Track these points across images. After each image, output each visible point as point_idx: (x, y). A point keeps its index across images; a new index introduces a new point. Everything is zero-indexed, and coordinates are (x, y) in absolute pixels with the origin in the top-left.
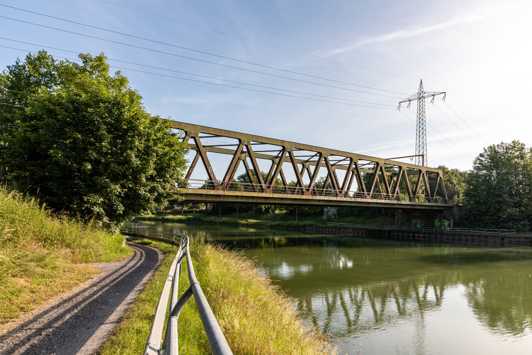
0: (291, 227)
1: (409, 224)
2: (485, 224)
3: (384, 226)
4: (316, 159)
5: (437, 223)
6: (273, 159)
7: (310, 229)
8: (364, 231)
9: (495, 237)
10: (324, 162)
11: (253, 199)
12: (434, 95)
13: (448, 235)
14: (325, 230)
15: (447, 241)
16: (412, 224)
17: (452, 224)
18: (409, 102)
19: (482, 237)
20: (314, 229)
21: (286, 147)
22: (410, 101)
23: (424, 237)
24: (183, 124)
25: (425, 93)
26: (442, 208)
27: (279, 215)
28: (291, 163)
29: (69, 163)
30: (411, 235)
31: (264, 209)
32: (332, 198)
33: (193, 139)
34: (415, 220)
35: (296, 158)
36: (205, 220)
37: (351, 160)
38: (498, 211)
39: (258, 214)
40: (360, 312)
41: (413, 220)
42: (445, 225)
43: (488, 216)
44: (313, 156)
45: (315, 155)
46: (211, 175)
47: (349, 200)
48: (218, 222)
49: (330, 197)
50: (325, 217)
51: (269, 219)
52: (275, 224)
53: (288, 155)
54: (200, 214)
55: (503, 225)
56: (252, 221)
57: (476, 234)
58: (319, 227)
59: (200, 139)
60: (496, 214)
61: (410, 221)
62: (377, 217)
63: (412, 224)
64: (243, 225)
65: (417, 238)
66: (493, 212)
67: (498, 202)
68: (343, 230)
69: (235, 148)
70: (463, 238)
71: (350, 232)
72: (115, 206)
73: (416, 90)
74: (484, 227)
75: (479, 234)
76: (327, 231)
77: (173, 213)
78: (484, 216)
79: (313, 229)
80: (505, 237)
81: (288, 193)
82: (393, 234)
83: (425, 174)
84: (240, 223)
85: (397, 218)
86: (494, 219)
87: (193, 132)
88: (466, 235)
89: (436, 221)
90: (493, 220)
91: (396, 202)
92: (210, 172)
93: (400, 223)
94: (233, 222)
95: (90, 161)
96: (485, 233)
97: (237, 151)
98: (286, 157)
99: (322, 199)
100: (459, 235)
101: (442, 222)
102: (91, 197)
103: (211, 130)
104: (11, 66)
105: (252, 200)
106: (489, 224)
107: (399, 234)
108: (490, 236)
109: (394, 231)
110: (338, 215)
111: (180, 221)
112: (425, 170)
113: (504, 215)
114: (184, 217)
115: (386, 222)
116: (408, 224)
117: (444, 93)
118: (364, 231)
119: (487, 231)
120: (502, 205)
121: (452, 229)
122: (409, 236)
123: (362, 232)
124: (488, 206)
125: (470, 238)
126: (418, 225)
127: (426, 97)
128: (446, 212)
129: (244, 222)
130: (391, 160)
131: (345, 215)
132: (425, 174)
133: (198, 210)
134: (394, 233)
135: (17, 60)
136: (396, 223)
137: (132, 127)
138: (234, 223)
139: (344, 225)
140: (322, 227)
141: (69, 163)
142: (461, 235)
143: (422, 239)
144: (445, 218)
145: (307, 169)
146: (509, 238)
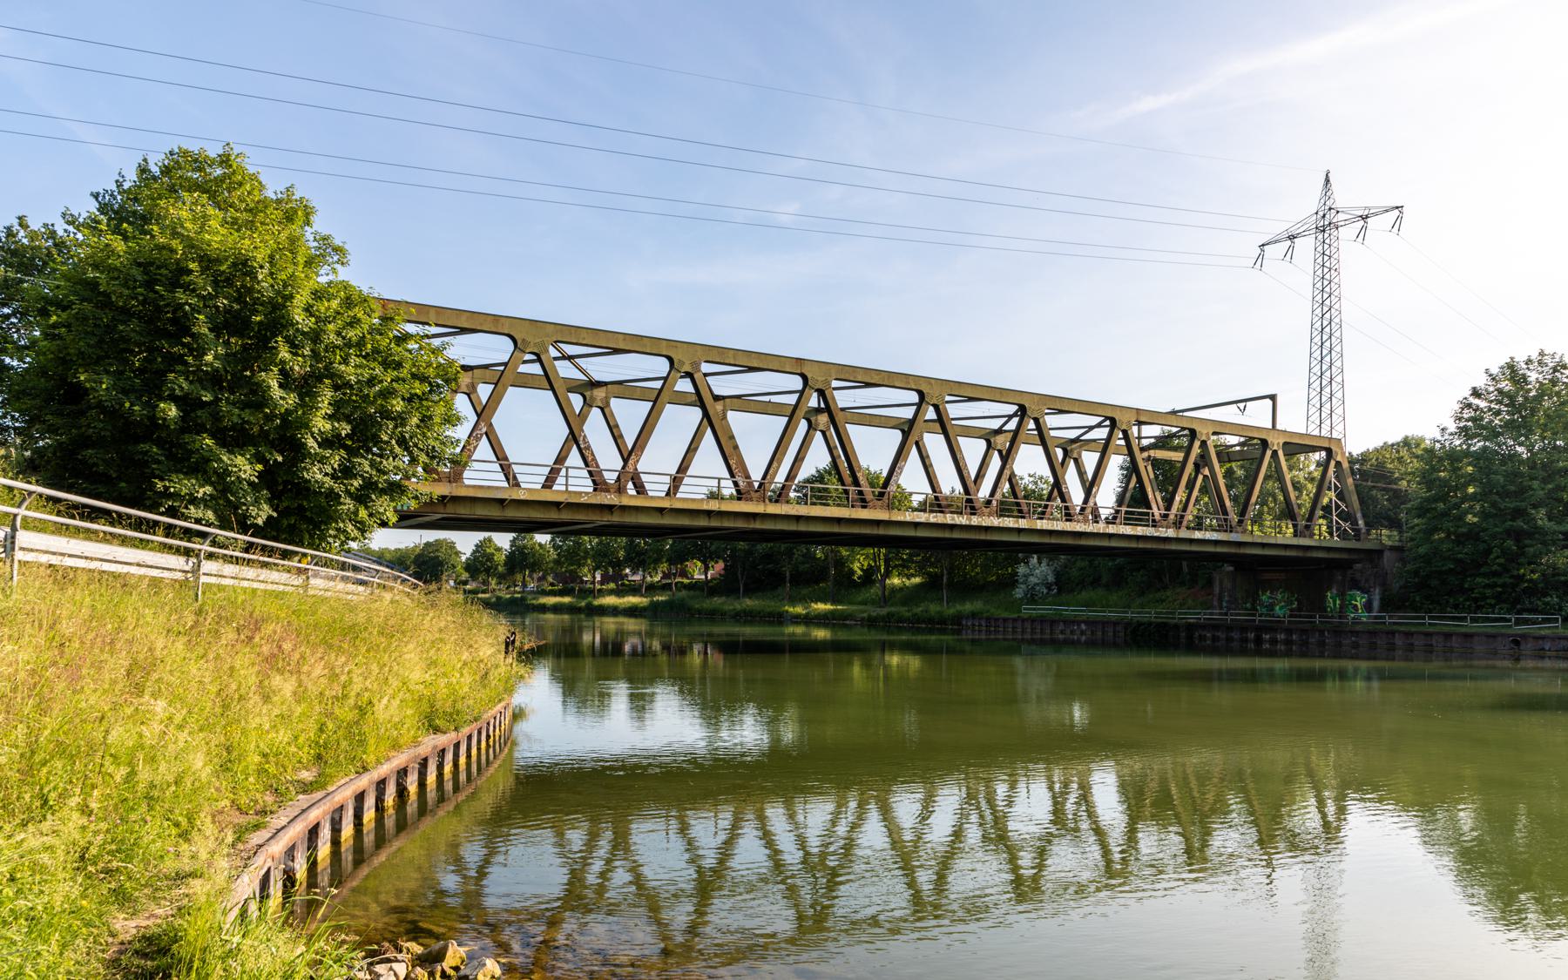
0: (924, 622)
1: (1253, 605)
2: (1476, 600)
3: (1173, 613)
4: (1102, 433)
5: (1332, 601)
6: (989, 436)
7: (974, 625)
8: (1119, 628)
9: (1494, 636)
10: (1122, 442)
11: (710, 518)
12: (1367, 217)
13: (1356, 633)
14: (1013, 628)
15: (1353, 651)
16: (1262, 605)
17: (1376, 604)
18: (1289, 242)
19: (1454, 638)
20: (983, 623)
21: (809, 376)
22: (1292, 238)
23: (1288, 642)
24: (504, 319)
25: (1338, 212)
26: (1344, 556)
27: (901, 589)
28: (1041, 448)
29: (127, 405)
30: (1252, 636)
31: (860, 572)
32: (953, 519)
33: (688, 380)
34: (1268, 593)
35: (1053, 433)
36: (697, 606)
37: (1113, 423)
38: (1513, 559)
39: (844, 585)
40: (936, 799)
41: (1264, 592)
42: (1356, 606)
43: (1484, 575)
44: (1091, 428)
45: (1099, 425)
46: (586, 453)
47: (1011, 525)
48: (730, 611)
49: (948, 515)
50: (1019, 592)
51: (873, 602)
52: (882, 613)
53: (935, 417)
54: (692, 593)
55: (1531, 603)
56: (821, 607)
57: (1437, 629)
58: (997, 620)
59: (834, 392)
60: (1508, 571)
61: (1255, 598)
62: (1165, 588)
63: (1262, 605)
64: (797, 620)
65: (1268, 646)
66: (1499, 565)
67: (1518, 535)
68: (1061, 626)
69: (791, 399)
70: (1399, 641)
71: (1082, 633)
72: (244, 508)
73: (1310, 203)
74: (1473, 609)
75: (1446, 629)
76: (1019, 630)
77: (622, 591)
78: (1471, 576)
79: (980, 625)
80: (1524, 636)
81: (853, 506)
82: (1200, 636)
83: (1280, 453)
84: (787, 612)
85: (1217, 590)
86: (1504, 585)
87: (533, 340)
88: (1408, 634)
89: (1329, 594)
90: (1500, 589)
91: (1171, 533)
92: (582, 446)
93: (1227, 602)
94: (768, 610)
95: (173, 398)
96: (1469, 626)
97: (661, 390)
98: (926, 421)
99: (923, 520)
100: (1388, 633)
101: (1348, 598)
102: (175, 483)
103: (584, 333)
104: (102, 192)
105: (707, 519)
106: (1488, 601)
107: (1216, 634)
108: (1478, 635)
109: (1203, 627)
110: (1056, 584)
111: (632, 612)
112: (1281, 441)
113: (1533, 572)
114: (645, 600)
115: (1190, 601)
116: (1248, 605)
117: (1397, 208)
118: (1119, 628)
119: (1474, 620)
120: (1527, 542)
121: (1376, 617)
122: (1246, 640)
123: (1114, 632)
124: (1482, 547)
125: (1418, 642)
126: (1277, 608)
127: (1343, 223)
128: (1358, 566)
129: (799, 610)
130: (1185, 414)
131: (1077, 585)
132: (1280, 453)
133: (686, 581)
134: (1204, 633)
135: (118, 178)
136: (1215, 603)
137: (277, 320)
138: (771, 615)
139: (1069, 611)
140: (1005, 620)
141: (127, 405)
142: (1393, 633)
143: (1283, 648)
144: (1355, 585)
145: (1076, 461)
146: (1537, 638)
